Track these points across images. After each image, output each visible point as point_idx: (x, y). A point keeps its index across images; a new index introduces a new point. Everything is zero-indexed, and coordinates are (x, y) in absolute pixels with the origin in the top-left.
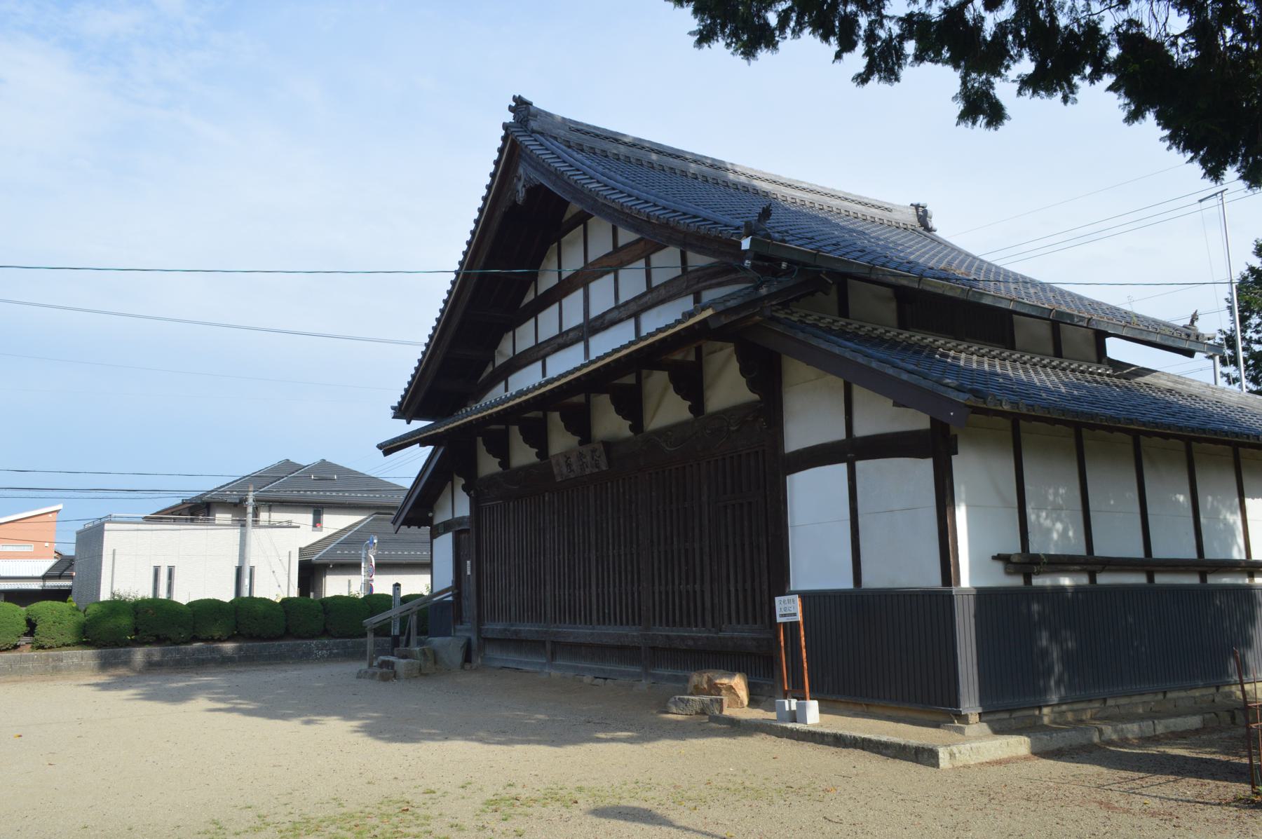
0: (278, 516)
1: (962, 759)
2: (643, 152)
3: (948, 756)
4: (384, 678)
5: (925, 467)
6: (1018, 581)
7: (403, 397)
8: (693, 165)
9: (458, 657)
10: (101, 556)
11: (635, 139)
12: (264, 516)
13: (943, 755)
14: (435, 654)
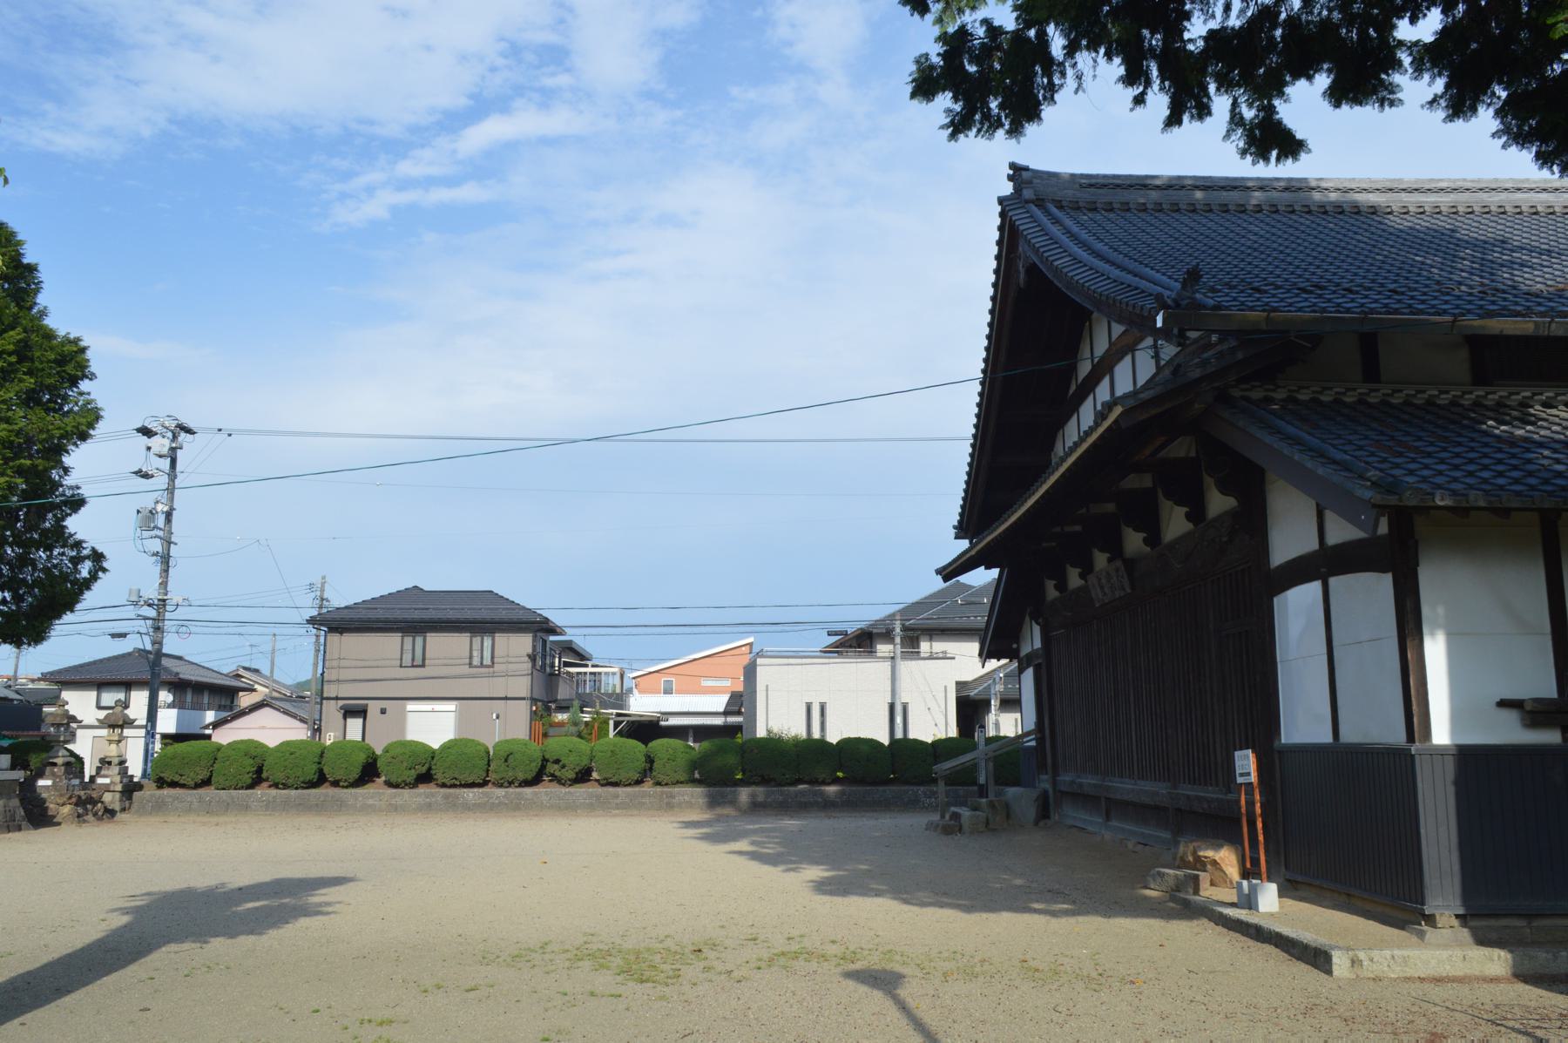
0: (939, 646)
1: (1369, 970)
2: (1182, 193)
3: (1348, 963)
4: (947, 831)
5: (1382, 585)
7: (961, 515)
8: (1257, 194)
9: (1032, 813)
11: (1172, 178)
12: (925, 646)
13: (1340, 961)
14: (1007, 806)
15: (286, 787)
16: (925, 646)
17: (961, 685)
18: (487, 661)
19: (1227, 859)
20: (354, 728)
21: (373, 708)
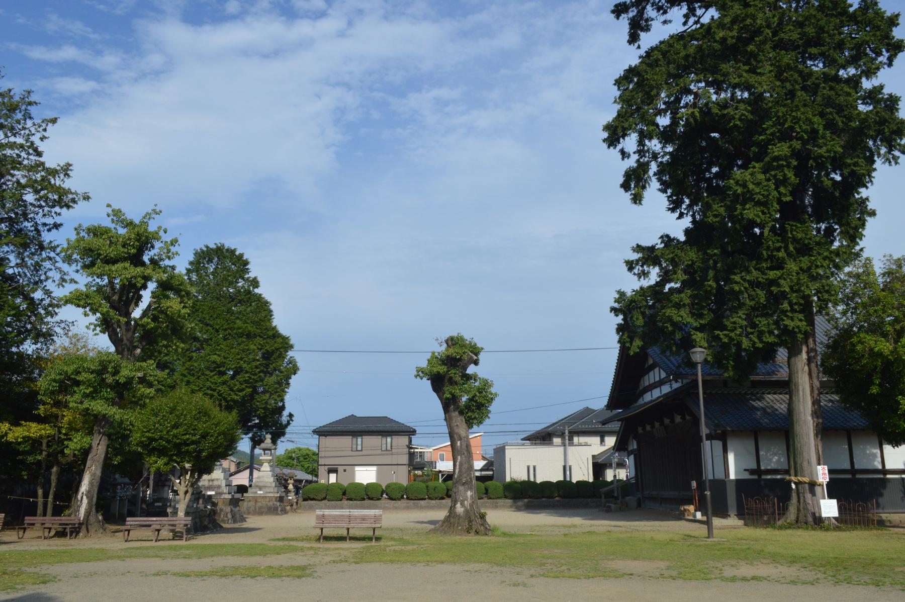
0: (583, 439)
6: (756, 477)
10: (505, 461)
12: (576, 439)
15: (355, 500)
16: (576, 439)
17: (594, 457)
18: (359, 448)
19: (691, 508)
20: (333, 478)
21: (341, 469)
